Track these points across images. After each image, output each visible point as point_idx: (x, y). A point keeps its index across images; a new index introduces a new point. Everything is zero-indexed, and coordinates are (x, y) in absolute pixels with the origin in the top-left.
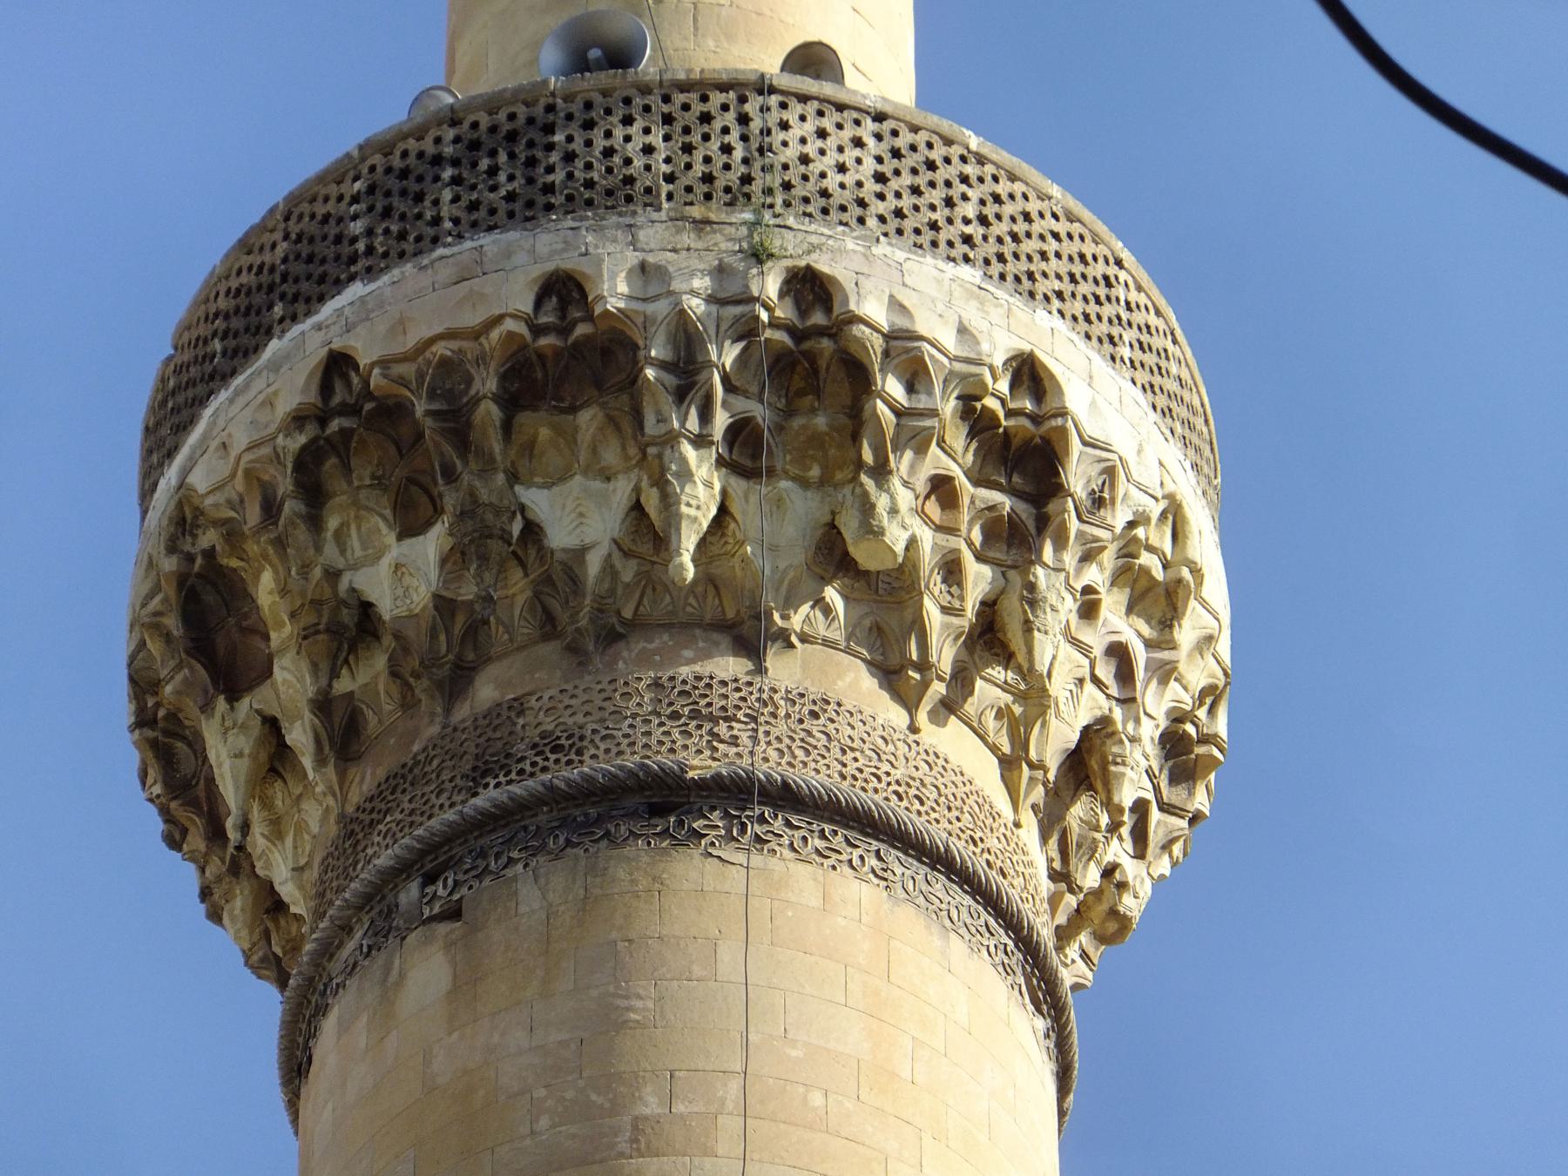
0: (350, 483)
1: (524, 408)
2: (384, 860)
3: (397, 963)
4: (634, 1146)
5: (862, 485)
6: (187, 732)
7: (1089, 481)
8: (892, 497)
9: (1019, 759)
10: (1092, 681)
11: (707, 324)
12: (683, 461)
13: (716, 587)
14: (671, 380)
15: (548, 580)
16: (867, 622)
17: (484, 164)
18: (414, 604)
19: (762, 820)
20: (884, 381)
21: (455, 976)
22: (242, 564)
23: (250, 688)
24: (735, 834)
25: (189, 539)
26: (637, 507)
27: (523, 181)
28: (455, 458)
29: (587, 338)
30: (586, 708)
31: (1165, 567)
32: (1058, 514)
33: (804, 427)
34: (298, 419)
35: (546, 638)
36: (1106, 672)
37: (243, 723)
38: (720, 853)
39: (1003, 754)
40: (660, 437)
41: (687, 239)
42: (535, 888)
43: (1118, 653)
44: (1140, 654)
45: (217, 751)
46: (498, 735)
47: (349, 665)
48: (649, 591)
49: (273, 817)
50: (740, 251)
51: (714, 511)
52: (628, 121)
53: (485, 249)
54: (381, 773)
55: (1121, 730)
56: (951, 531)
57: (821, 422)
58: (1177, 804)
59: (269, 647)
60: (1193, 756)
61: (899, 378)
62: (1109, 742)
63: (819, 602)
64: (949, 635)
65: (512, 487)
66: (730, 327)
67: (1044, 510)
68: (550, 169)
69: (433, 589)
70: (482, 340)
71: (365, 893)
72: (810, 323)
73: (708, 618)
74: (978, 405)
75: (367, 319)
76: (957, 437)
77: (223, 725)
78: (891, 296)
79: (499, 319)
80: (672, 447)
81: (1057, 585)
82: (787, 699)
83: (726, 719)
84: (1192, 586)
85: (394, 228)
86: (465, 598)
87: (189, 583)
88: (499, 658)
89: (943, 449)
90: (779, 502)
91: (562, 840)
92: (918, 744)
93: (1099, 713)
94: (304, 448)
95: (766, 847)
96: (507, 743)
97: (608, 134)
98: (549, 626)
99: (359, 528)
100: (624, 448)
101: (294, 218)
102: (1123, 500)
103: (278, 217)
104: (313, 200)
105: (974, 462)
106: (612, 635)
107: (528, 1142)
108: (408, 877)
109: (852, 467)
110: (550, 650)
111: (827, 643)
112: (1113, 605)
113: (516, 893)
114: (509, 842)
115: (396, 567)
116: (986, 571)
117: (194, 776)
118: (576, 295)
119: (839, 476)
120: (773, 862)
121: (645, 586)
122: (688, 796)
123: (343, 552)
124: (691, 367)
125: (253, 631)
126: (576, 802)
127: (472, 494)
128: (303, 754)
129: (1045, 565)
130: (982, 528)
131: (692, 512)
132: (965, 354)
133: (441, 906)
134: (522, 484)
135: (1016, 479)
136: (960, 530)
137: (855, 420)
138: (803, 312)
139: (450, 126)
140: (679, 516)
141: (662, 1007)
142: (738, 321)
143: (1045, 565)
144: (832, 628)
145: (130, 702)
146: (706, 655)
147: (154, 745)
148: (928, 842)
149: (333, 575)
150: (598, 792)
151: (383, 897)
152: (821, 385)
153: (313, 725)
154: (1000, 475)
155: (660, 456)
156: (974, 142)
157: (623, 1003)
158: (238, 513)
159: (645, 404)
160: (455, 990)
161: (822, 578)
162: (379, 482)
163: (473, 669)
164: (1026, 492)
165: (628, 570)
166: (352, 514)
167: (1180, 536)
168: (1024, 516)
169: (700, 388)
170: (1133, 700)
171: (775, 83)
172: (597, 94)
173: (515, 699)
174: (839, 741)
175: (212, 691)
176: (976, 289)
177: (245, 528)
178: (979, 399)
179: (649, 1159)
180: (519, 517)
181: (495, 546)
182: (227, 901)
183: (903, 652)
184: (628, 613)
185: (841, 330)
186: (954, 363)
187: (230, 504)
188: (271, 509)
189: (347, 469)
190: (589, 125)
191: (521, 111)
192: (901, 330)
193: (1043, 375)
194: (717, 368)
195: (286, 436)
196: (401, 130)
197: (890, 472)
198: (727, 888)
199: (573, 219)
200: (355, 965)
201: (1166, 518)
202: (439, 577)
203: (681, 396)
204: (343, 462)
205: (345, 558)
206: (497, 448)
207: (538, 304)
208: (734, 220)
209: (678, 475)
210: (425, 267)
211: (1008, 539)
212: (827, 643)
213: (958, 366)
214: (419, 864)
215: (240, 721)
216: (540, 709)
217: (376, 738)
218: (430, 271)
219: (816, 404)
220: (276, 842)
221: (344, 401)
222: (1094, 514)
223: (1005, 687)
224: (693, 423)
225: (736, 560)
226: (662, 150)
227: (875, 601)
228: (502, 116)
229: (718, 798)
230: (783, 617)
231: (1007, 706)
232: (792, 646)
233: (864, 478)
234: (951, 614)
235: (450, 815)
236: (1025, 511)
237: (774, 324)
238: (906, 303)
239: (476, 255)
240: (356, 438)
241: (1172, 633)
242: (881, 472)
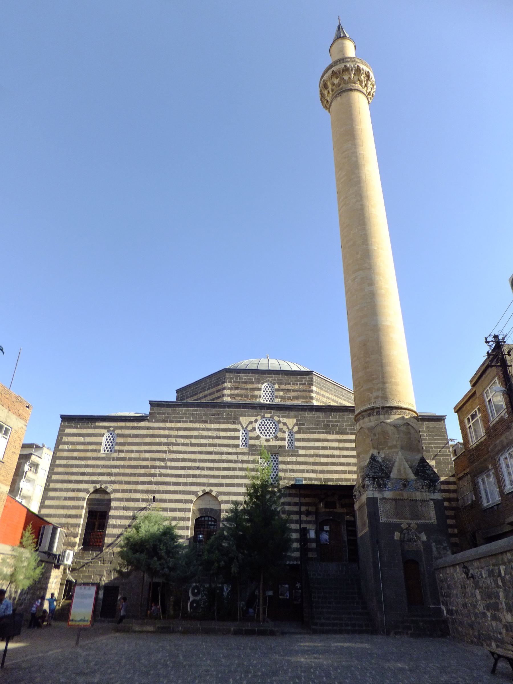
43: (371, 88)
98: (344, 83)
106: (348, 83)
112: (371, 85)
160: (341, 99)
188: (329, 79)
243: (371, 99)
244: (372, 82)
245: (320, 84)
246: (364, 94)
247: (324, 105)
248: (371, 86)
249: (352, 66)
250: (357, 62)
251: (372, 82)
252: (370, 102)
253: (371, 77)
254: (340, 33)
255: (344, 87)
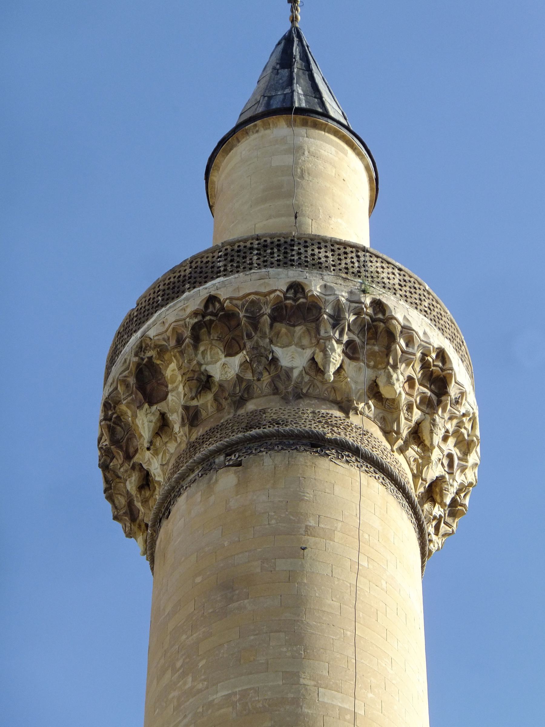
0: (210, 338)
1: (278, 322)
2: (211, 448)
3: (214, 478)
4: (306, 533)
5: (388, 369)
6: (123, 424)
7: (455, 394)
8: (398, 375)
9: (419, 476)
10: (441, 464)
11: (346, 306)
12: (333, 345)
13: (335, 391)
14: (331, 321)
15: (278, 376)
16: (381, 415)
17: (269, 251)
18: (228, 377)
19: (348, 456)
20: (400, 340)
21: (239, 480)
22: (162, 362)
23: (157, 403)
24: (340, 457)
25: (142, 353)
26: (313, 359)
27: (283, 257)
28: (252, 331)
29: (304, 303)
30: (289, 414)
31: (468, 435)
32: (445, 401)
33: (370, 349)
34: (195, 314)
35: (274, 394)
36: (446, 462)
37: (153, 413)
38: (335, 461)
39: (414, 473)
40: (325, 337)
41: (340, 281)
42: (270, 459)
43: (450, 456)
44: (456, 461)
45: (143, 421)
46: (256, 418)
47: (197, 398)
48: (312, 386)
49: (155, 449)
50: (358, 289)
51: (339, 366)
52: (319, 248)
53: (270, 272)
54: (207, 428)
55: (448, 481)
56: (411, 396)
57: (376, 348)
58: (449, 523)
59: (167, 389)
60: (457, 509)
61: (404, 341)
62: (443, 484)
63: (367, 404)
64: (406, 426)
65: (270, 345)
66: (353, 309)
67: (441, 399)
68: (293, 256)
69: (237, 372)
70: (267, 297)
71: (203, 458)
72: (377, 317)
73: (331, 399)
74: (426, 358)
75: (225, 286)
76: (418, 366)
77: (146, 412)
78: (405, 316)
79: (275, 291)
80: (329, 341)
81: (442, 422)
82: (356, 428)
83: (337, 427)
84: (477, 442)
85: (235, 265)
86: (246, 378)
87: (140, 367)
88: (257, 398)
89: (413, 368)
90: (360, 368)
91: (280, 448)
92: (393, 455)
93: (442, 474)
94: (196, 323)
95: (350, 464)
96: (259, 421)
97: (313, 250)
99: (211, 352)
100: (311, 340)
101: (194, 263)
102: (463, 405)
103: (188, 262)
104: (202, 257)
105: (421, 377)
106: (299, 396)
107: (267, 526)
108: (220, 454)
109: (385, 364)
110: (276, 398)
111: (368, 417)
112: (451, 441)
113: (263, 460)
114: (260, 446)
115: (224, 364)
116: (419, 412)
117: (121, 439)
118: (300, 290)
119: (380, 366)
120: (352, 469)
121: (311, 385)
122: (325, 444)
123: (204, 358)
124: (339, 319)
125: (162, 384)
126: (286, 438)
127: (257, 342)
128: (176, 423)
129: (439, 415)
130: (420, 398)
131: (334, 361)
132: (425, 340)
133: (233, 462)
134: (273, 345)
135: (432, 386)
136: (413, 396)
137: (388, 350)
138: (375, 314)
139: (256, 240)
140: (330, 361)
141: (316, 497)
142: (356, 308)
143: (439, 415)
144: (370, 413)
145: (102, 412)
146: (330, 409)
147: (109, 427)
148: (399, 480)
149: (200, 364)
150: (294, 436)
151: (209, 460)
152: (378, 338)
153: (182, 413)
154: (428, 384)
155: (325, 343)
156: (427, 288)
157: (302, 494)
158: (167, 343)
159: (321, 326)
160: (238, 484)
161: (369, 397)
162: (220, 339)
163: (246, 400)
164: (435, 392)
165: (307, 378)
166: (209, 347)
167: (474, 428)
168: (434, 399)
169: (341, 325)
170: (453, 473)
171: (368, 249)
172: (309, 239)
173: (262, 409)
174: (372, 444)
175: (143, 401)
176: (429, 324)
177: (169, 347)
178: (427, 356)
179: (311, 537)
180: (271, 354)
181: (263, 359)
182: (129, 478)
183: (392, 427)
184: (304, 391)
185: (388, 321)
186: (422, 342)
187: (164, 339)
188: (180, 341)
189: (209, 333)
190: (306, 247)
191: (282, 240)
192: (407, 326)
193: (446, 357)
194: (348, 320)
195: (190, 319)
196: (238, 239)
197: (398, 368)
198: (337, 471)
199: (301, 269)
200: (195, 480)
201: (471, 420)
202: (239, 369)
203: (334, 327)
204: (208, 331)
205: (204, 361)
206: (267, 331)
207: (288, 290)
208: (356, 280)
209: (330, 349)
210: (248, 275)
211: (427, 405)
212: (368, 417)
213: (423, 343)
214: (225, 450)
215: (152, 412)
216: (272, 413)
217: (205, 420)
218: (249, 276)
219: (375, 343)
220: (155, 456)
221: (212, 311)
222: (455, 405)
223: (417, 453)
224: (337, 335)
225: (343, 383)
226: (331, 258)
227: (384, 410)
228: (276, 240)
229: (335, 447)
230: (357, 403)
231: (417, 459)
232: (357, 414)
233: (389, 367)
234: (408, 421)
235: (240, 435)
236: (434, 398)
237: (367, 314)
238: (409, 319)
239: (267, 273)
240: (214, 323)
241: (467, 457)
242: (395, 367)
243: (443, 528)
244: (460, 425)
245: (111, 361)
246: (401, 488)
247: (122, 501)
248: (450, 446)
249: (343, 297)
250: (374, 278)
251: (460, 425)
252: (433, 547)
253: (453, 391)
254: (290, 82)
255: (271, 415)
